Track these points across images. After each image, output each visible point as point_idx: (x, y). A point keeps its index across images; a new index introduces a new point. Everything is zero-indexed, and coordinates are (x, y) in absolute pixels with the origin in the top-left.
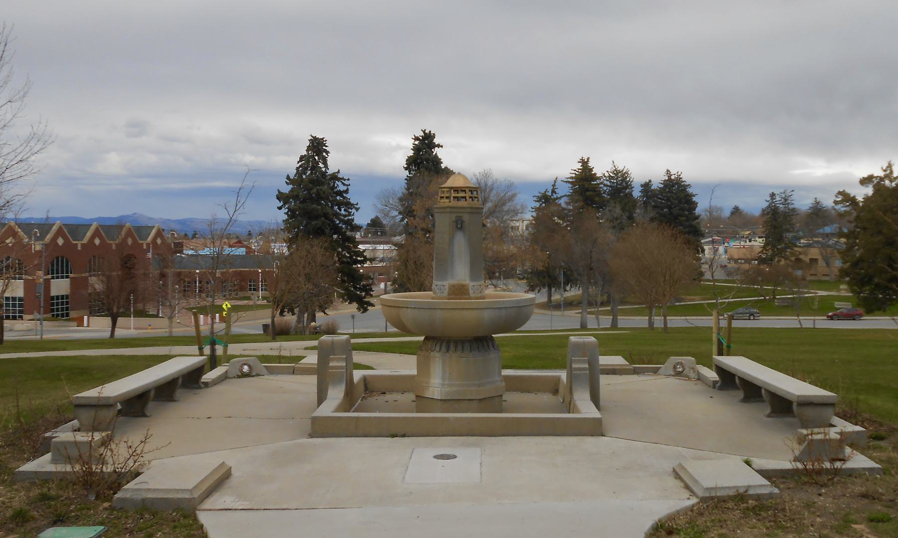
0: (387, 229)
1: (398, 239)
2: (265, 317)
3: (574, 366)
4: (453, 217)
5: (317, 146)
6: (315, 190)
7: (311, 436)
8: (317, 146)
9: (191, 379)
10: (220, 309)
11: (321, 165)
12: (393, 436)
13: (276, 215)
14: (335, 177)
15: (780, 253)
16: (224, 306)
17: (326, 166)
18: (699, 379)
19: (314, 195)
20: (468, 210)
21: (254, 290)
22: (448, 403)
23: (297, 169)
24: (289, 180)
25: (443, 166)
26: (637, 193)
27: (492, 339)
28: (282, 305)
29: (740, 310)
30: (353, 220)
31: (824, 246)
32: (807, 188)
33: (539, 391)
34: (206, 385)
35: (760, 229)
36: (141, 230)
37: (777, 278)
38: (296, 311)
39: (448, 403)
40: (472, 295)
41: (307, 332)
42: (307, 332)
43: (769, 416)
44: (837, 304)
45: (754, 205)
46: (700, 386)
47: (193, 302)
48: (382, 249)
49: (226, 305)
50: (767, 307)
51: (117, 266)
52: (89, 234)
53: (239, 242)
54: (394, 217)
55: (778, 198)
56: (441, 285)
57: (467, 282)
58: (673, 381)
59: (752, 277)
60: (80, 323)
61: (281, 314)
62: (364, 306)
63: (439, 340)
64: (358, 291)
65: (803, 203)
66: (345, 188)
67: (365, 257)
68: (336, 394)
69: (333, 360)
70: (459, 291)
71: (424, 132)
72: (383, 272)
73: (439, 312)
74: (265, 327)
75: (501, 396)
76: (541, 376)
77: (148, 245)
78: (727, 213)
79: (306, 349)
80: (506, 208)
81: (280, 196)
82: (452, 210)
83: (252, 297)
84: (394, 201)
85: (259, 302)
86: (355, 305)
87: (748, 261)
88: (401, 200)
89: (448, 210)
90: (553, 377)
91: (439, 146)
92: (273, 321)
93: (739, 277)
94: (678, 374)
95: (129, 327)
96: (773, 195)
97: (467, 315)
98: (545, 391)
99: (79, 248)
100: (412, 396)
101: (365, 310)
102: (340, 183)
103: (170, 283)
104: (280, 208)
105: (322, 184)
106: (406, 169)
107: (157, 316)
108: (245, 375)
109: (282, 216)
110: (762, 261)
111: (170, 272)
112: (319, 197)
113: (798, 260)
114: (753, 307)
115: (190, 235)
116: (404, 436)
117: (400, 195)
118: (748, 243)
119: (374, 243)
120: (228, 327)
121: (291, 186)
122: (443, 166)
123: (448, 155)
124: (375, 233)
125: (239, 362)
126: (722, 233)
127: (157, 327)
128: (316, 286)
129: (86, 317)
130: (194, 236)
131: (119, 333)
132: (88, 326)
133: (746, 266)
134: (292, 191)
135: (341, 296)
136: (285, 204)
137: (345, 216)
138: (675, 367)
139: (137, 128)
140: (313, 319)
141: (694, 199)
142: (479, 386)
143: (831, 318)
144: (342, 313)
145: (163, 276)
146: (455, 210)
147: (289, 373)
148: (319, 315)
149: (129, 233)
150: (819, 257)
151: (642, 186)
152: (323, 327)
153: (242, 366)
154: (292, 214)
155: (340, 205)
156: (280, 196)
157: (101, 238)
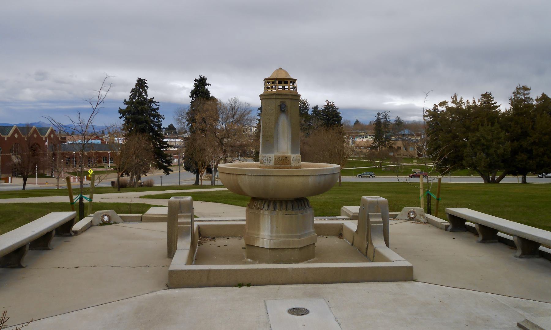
0: (177, 131)
1: (186, 135)
2: (114, 177)
3: (372, 220)
4: (278, 102)
5: (141, 84)
6: (140, 108)
7: (169, 287)
8: (141, 84)
9: (65, 230)
10: (87, 173)
11: (143, 94)
12: (240, 285)
13: (119, 122)
14: (151, 101)
15: (382, 143)
16: (89, 172)
17: (146, 95)
18: (428, 223)
19: (140, 111)
20: (290, 97)
21: (106, 163)
22: (277, 254)
23: (130, 96)
24: (126, 102)
25: (211, 95)
26: (310, 112)
27: (307, 200)
28: (122, 170)
29: (365, 173)
30: (161, 124)
31: (403, 140)
32: (394, 111)
33: (327, 235)
34: (76, 233)
35: (371, 131)
36: (41, 130)
37: (384, 157)
38: (130, 174)
39: (277, 254)
40: (293, 165)
41: (137, 186)
42: (137, 186)
43: (520, 257)
44: (413, 170)
45: (367, 119)
46: (434, 229)
47: (71, 170)
48: (177, 141)
49: (91, 171)
50: (379, 171)
51: (26, 150)
52: (11, 132)
53: (97, 137)
54: (184, 123)
55: (381, 115)
56: (268, 157)
57: (289, 154)
58: (409, 224)
59: (371, 156)
60: (6, 181)
61: (122, 176)
62: (167, 171)
63: (259, 200)
64: (163, 162)
65: (392, 119)
66: (157, 107)
67: (168, 145)
68: (184, 246)
69: (181, 217)
70: (283, 162)
71: (201, 77)
72: (177, 153)
73: (272, 179)
74: (113, 183)
75: (314, 244)
76: (332, 224)
77: (46, 138)
78: (352, 124)
79: (140, 197)
80: (245, 118)
81: (121, 111)
82: (278, 97)
83: (105, 166)
84: (184, 114)
85: (109, 170)
86: (162, 171)
87: (366, 148)
88: (188, 113)
89: (274, 97)
90: (338, 225)
91: (208, 84)
92: (118, 180)
93: (362, 156)
94: (412, 219)
95: (34, 183)
96: (379, 114)
97: (288, 180)
98: (332, 235)
99: (6, 139)
100: (243, 243)
101: (168, 173)
102: (154, 104)
103: (58, 159)
104: (120, 118)
105: (145, 104)
106: (191, 97)
107: (51, 177)
108: (105, 223)
109: (122, 121)
110: (372, 148)
111: (58, 152)
112: (142, 112)
113: (391, 147)
114: (372, 171)
115: (70, 133)
116: (249, 285)
117: (187, 111)
118: (365, 139)
119: (170, 138)
120: (92, 183)
121: (127, 106)
122: (211, 95)
123: (214, 90)
124: (170, 133)
125: (101, 213)
126: (351, 133)
127: (49, 183)
128: (141, 160)
129: (10, 178)
130: (72, 134)
131: (28, 186)
132: (11, 182)
133: (365, 151)
134: (127, 108)
135: (155, 166)
136: (123, 115)
137: (157, 122)
138: (409, 214)
139: (42, 75)
140: (139, 178)
141: (340, 115)
142: (300, 237)
143: (411, 177)
144: (155, 176)
145: (54, 155)
146: (280, 97)
147: (138, 221)
148: (143, 176)
149: (35, 131)
150: (402, 146)
151: (313, 108)
152: (145, 183)
153: (103, 217)
154: (127, 121)
155: (154, 116)
156: (121, 111)
157: (18, 134)
